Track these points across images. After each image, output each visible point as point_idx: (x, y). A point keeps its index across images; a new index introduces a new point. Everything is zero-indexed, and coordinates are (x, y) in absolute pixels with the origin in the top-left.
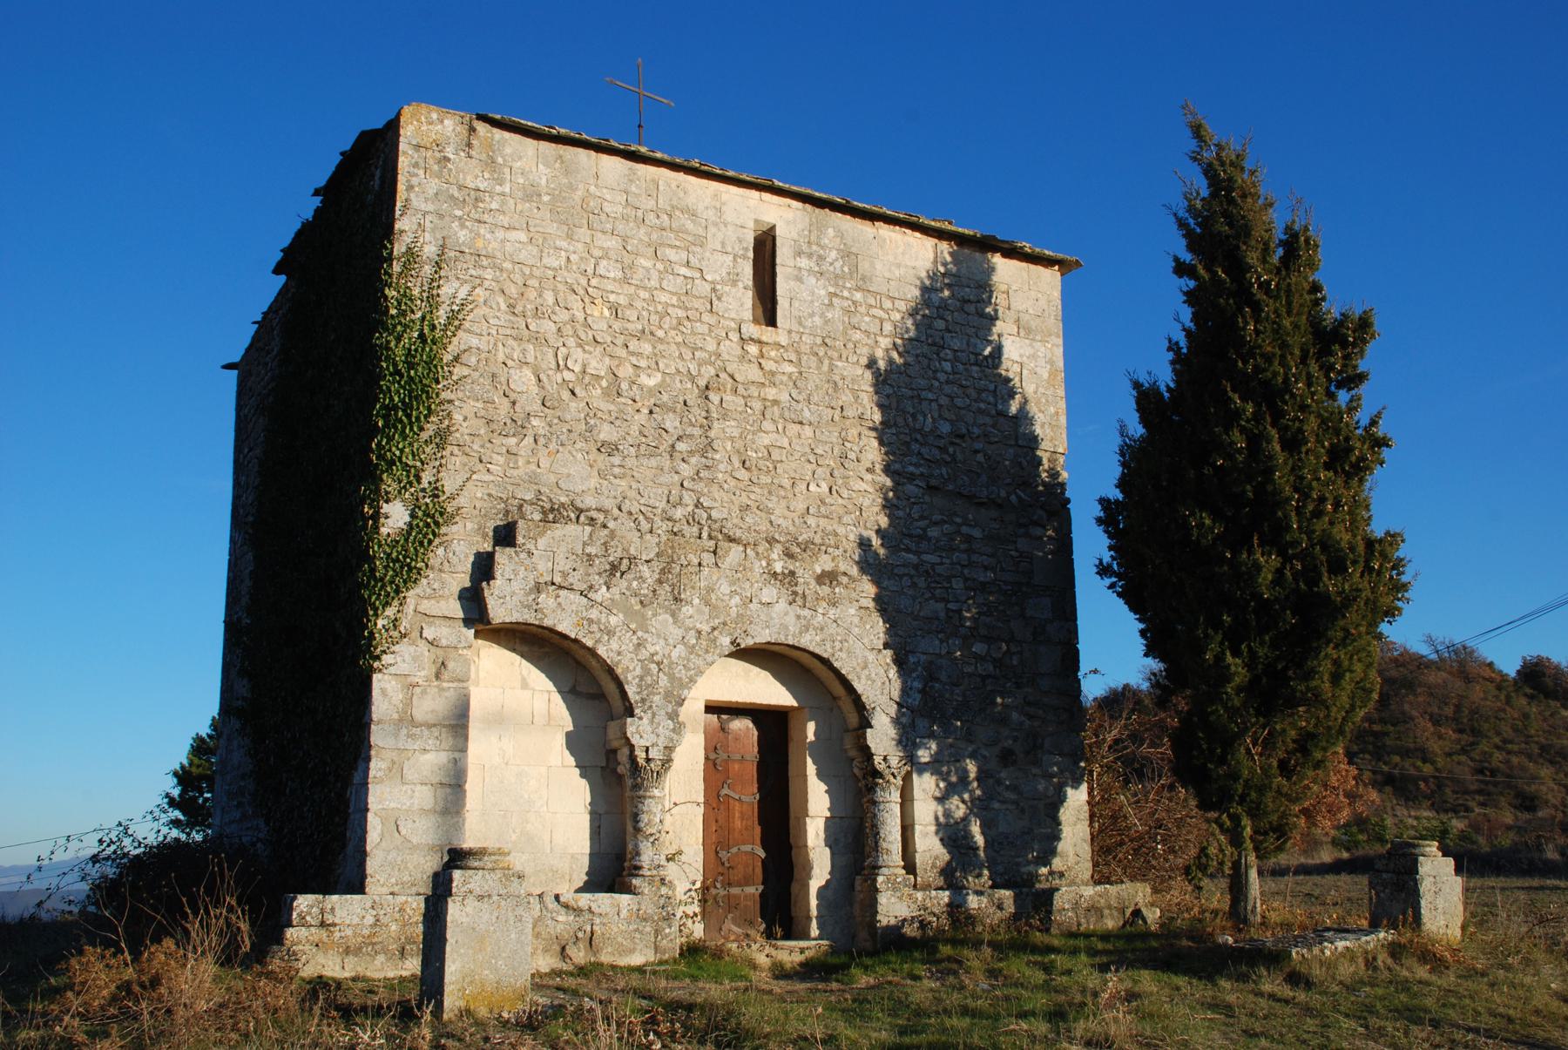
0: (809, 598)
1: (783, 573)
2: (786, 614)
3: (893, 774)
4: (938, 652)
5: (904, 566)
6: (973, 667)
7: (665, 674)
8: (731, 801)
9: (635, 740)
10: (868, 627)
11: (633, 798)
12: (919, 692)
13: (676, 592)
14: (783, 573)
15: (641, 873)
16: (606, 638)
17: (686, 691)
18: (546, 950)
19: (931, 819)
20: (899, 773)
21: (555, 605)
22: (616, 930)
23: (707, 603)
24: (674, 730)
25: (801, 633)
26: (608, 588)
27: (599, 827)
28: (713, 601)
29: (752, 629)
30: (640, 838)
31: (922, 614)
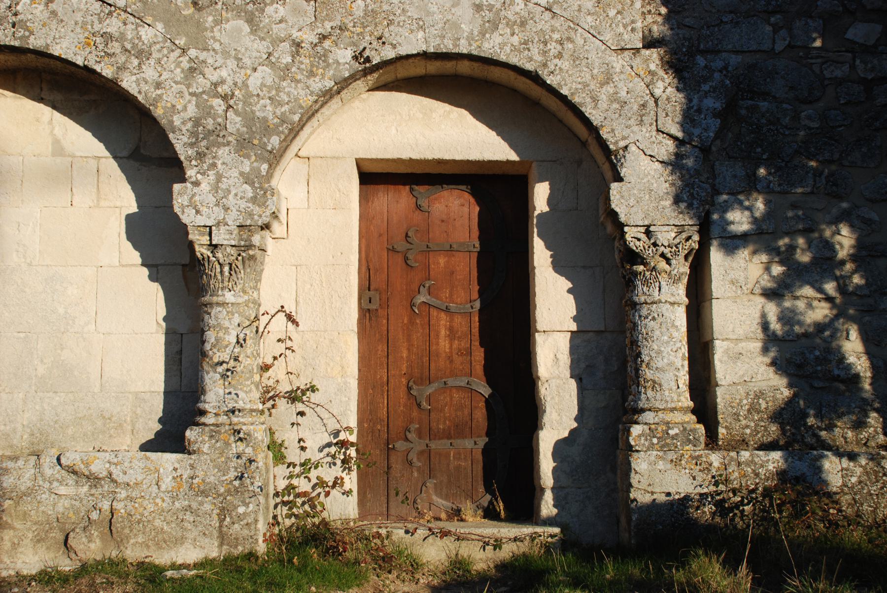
3: (663, 255)
4: (767, 46)
6: (846, 68)
7: (237, 113)
8: (434, 312)
9: (188, 217)
10: (612, 13)
12: (716, 115)
16: (136, 62)
18: (39, 540)
21: (46, 14)
22: (151, 507)
24: (254, 200)
25: (483, 34)
27: (180, 352)
29: (393, 34)
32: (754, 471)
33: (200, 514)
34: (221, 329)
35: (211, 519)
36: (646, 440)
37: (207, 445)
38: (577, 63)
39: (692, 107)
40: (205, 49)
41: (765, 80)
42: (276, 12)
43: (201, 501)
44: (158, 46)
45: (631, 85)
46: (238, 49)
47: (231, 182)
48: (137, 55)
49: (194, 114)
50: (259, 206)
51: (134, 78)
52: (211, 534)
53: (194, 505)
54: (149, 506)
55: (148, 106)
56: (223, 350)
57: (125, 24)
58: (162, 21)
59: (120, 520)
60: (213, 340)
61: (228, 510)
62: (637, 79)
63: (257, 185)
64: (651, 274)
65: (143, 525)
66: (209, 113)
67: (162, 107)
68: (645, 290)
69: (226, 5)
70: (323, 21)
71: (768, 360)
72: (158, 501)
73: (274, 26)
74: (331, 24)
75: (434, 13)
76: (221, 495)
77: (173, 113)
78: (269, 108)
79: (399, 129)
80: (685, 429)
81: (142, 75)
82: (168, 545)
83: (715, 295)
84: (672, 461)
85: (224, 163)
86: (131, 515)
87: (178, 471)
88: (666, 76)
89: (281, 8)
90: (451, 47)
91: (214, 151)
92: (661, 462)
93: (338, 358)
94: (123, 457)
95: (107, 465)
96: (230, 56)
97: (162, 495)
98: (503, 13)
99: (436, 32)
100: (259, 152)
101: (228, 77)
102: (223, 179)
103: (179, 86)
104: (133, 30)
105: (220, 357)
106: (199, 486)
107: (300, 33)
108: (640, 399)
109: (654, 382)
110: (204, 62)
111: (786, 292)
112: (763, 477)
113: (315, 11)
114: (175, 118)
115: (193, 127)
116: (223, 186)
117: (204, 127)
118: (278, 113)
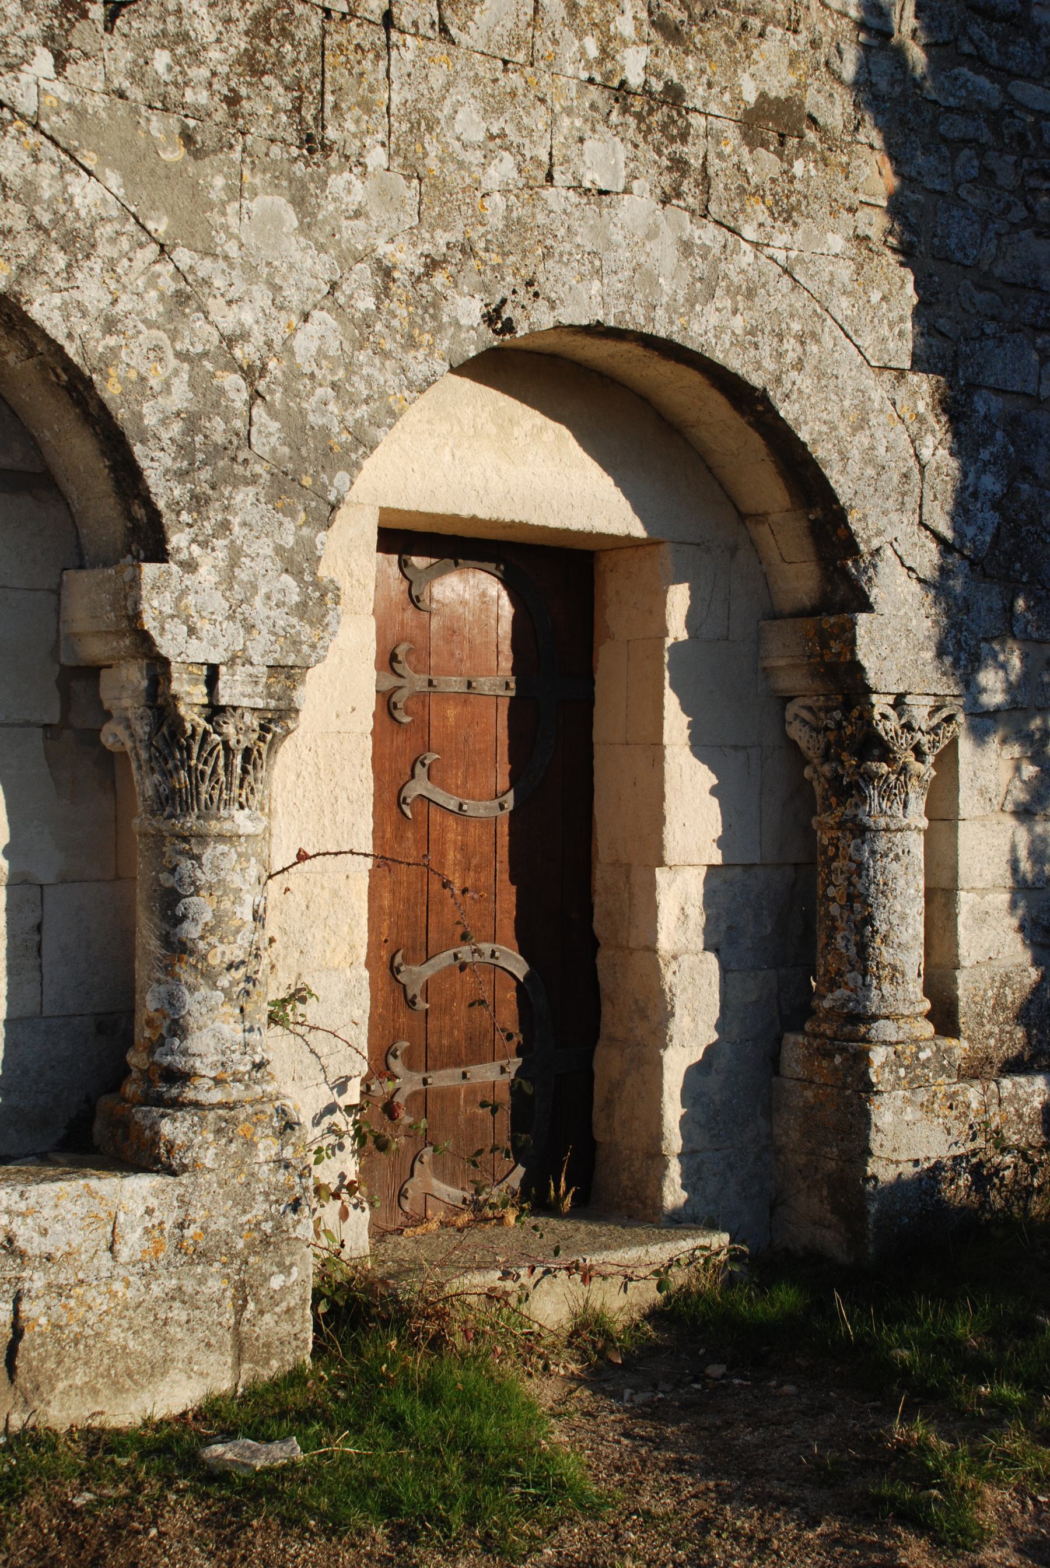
0: (718, 187)
1: (647, 91)
2: (652, 234)
4: (1030, 389)
5: (962, 111)
7: (270, 409)
8: (436, 816)
10: (876, 297)
11: (159, 839)
13: (308, 114)
14: (647, 91)
15: (190, 1094)
16: (61, 260)
17: (341, 477)
19: (1001, 873)
20: (933, 745)
22: (102, 1303)
23: (414, 173)
24: (301, 610)
25: (691, 302)
26: (61, 62)
27: (39, 928)
28: (432, 163)
30: (186, 975)
31: (998, 271)
32: (1017, 1111)
33: (201, 1304)
34: (225, 893)
35: (222, 1310)
36: (891, 1072)
37: (212, 1151)
38: (823, 382)
39: (967, 487)
40: (208, 253)
41: (1029, 446)
42: (349, 192)
43: (202, 1274)
44: (108, 229)
45: (892, 436)
46: (276, 263)
47: (259, 568)
48: (62, 242)
49: (185, 405)
50: (311, 624)
51: (57, 299)
52: (221, 1343)
53: (189, 1286)
54: (99, 1301)
55: (88, 373)
56: (231, 939)
57: (37, 160)
58: (119, 169)
59: (39, 1341)
60: (207, 917)
61: (251, 1287)
62: (900, 427)
63: (307, 578)
64: (897, 779)
65: (86, 1346)
66: (216, 405)
67: (118, 377)
68: (884, 806)
69: (250, 155)
70: (432, 228)
71: (1015, 922)
72: (118, 1286)
73: (345, 223)
74: (448, 237)
75: (619, 246)
76: (237, 1256)
77: (143, 395)
78: (333, 407)
79: (458, 454)
80: (938, 1049)
81: (75, 293)
82: (136, 1383)
83: (963, 813)
84: (922, 1105)
85: (244, 524)
86: (60, 1327)
87: (157, 1213)
88: (937, 427)
89: (358, 184)
90: (642, 322)
91: (227, 494)
92: (909, 1109)
93: (346, 929)
94: (40, 1196)
95: (5, 1220)
96: (258, 276)
97: (122, 1272)
98: (723, 266)
99: (620, 285)
100: (313, 504)
101: (255, 327)
102: (243, 559)
103: (155, 332)
104: (53, 177)
105: (224, 953)
106: (196, 1242)
107: (390, 248)
108: (867, 998)
109: (894, 968)
110: (206, 282)
111: (1039, 808)
112: (1027, 1120)
113: (420, 203)
114: (146, 408)
115: (185, 433)
116: (242, 575)
117: (206, 437)
118: (350, 422)
